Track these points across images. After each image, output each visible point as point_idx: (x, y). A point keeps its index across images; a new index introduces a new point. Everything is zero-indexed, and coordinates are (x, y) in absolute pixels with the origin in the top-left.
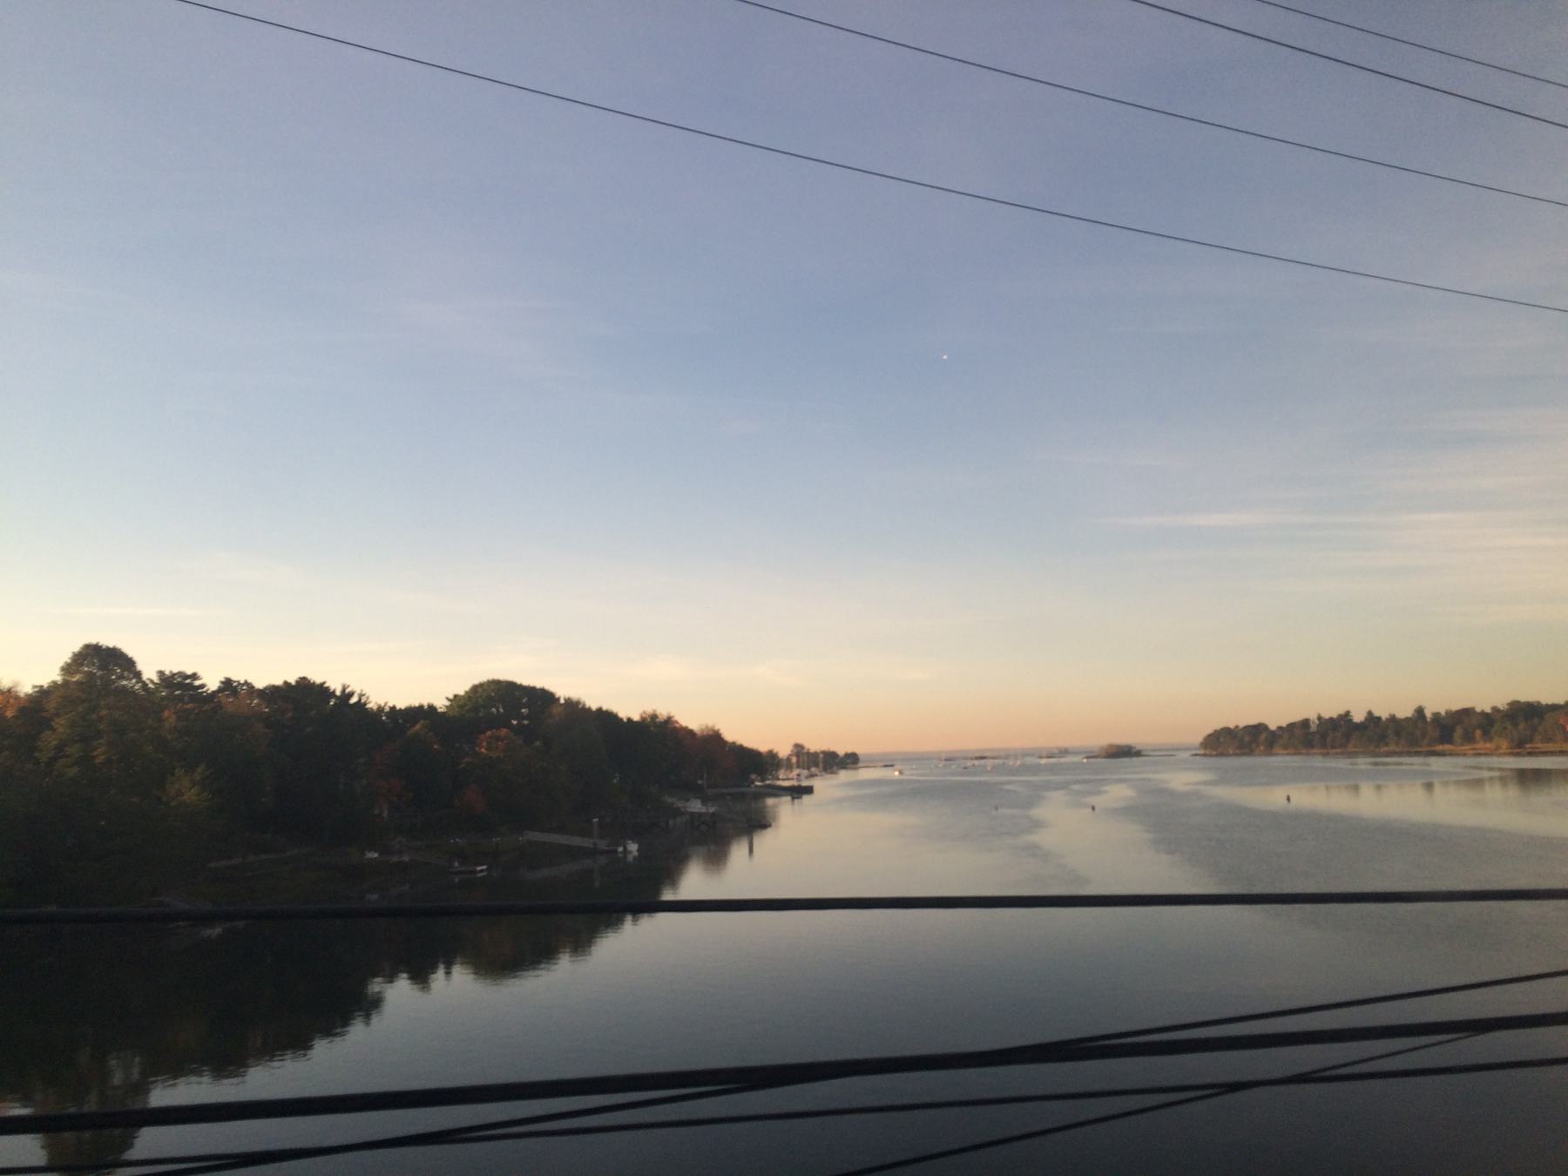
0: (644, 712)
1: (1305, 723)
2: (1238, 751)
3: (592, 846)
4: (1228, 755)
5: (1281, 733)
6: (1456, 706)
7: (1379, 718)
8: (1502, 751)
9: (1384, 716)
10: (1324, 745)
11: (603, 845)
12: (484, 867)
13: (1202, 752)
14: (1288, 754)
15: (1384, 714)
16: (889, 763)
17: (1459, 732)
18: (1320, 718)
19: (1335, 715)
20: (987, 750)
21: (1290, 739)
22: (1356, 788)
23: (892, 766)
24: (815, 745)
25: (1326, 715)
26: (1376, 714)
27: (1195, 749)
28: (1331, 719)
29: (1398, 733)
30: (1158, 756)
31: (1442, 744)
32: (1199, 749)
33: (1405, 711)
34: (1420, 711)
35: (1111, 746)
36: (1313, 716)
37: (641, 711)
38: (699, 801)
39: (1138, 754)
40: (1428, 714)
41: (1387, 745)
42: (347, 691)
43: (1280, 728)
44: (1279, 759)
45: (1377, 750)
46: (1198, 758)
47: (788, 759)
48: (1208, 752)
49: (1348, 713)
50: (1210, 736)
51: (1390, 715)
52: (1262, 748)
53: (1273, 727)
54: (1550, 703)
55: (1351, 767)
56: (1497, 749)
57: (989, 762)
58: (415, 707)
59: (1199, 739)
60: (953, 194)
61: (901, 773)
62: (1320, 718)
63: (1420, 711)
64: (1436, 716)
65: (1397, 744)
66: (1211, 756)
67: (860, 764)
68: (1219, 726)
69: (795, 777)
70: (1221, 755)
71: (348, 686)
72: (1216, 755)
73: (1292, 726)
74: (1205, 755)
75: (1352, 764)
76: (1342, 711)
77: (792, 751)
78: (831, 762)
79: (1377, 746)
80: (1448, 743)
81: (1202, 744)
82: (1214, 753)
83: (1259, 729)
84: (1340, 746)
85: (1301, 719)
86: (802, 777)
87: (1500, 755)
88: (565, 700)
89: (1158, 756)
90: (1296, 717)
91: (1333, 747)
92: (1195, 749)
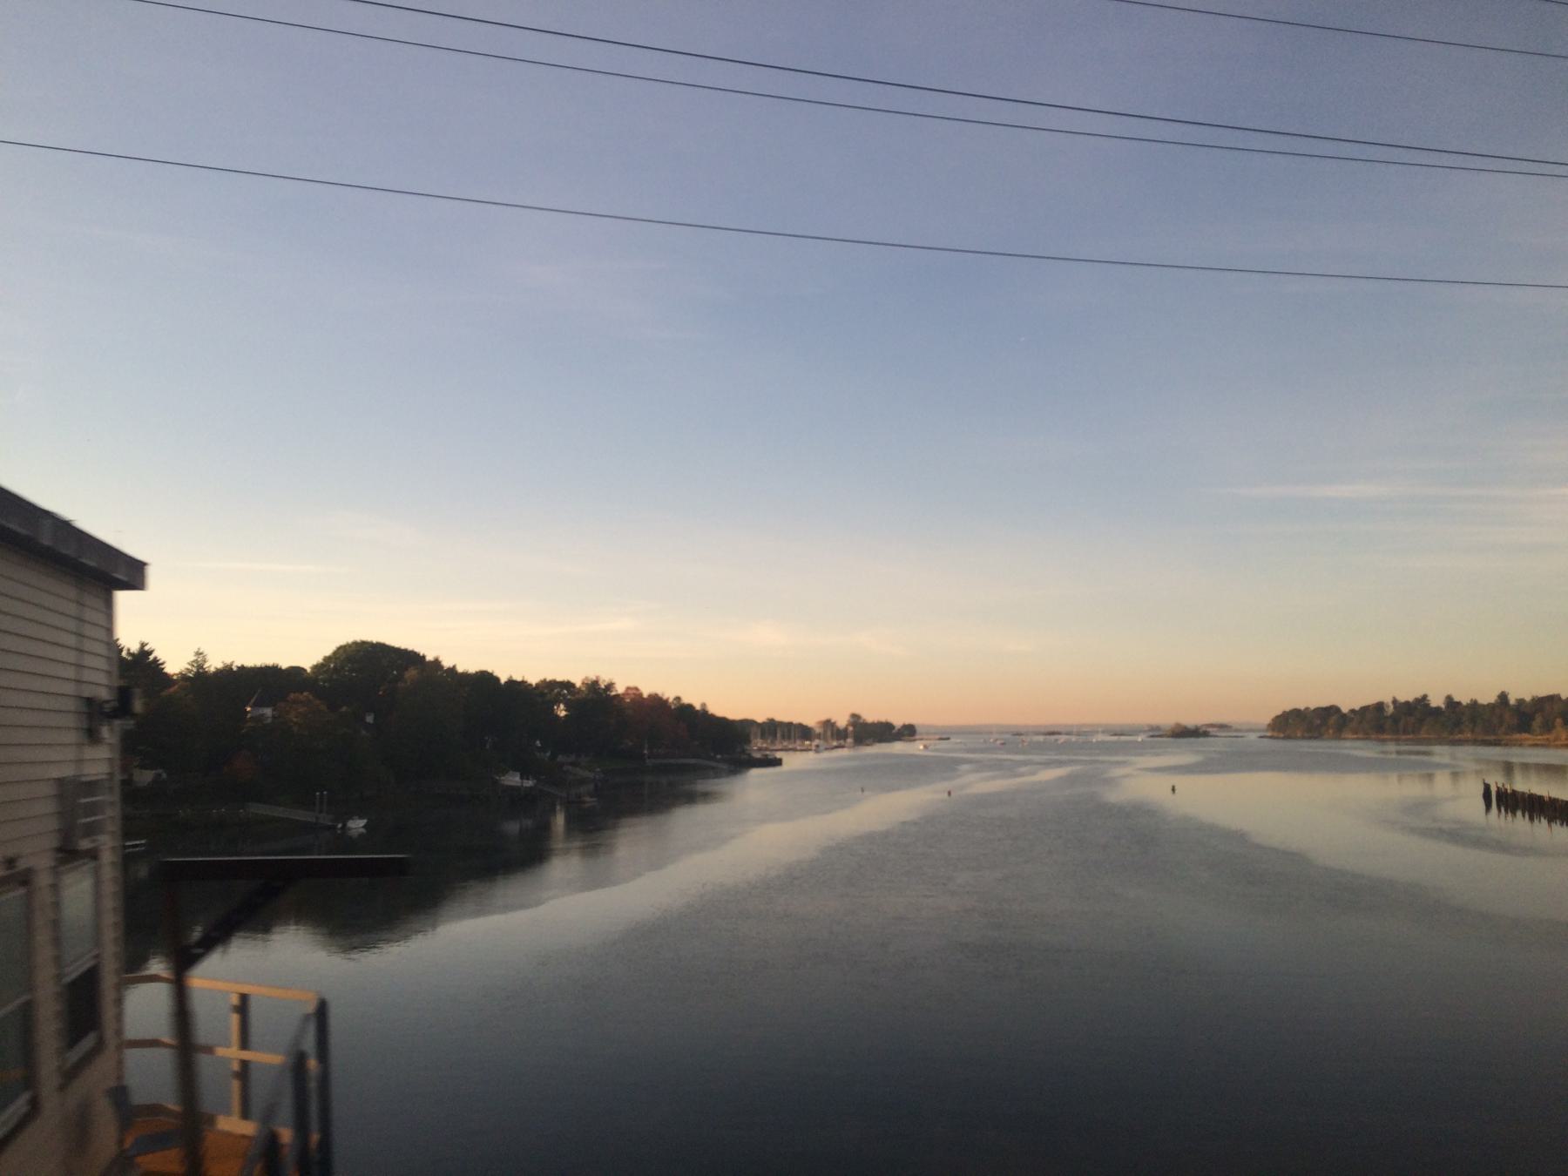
0: (587, 678)
1: (1380, 707)
2: (1306, 735)
3: (314, 820)
4: (1296, 738)
5: (1353, 716)
6: (1543, 692)
7: (1459, 703)
8: (1559, 743)
9: (1465, 700)
10: (1396, 732)
11: (325, 819)
12: (143, 842)
13: (1269, 734)
14: (1358, 739)
15: (1463, 698)
16: (944, 736)
17: (1537, 722)
18: (1395, 701)
19: (1411, 699)
20: (1084, 725)
21: (1361, 722)
22: (1430, 777)
23: (948, 739)
24: (870, 716)
25: (1402, 698)
26: (1456, 699)
27: (1263, 731)
28: (1407, 703)
29: (1473, 720)
30: (1226, 737)
31: (1520, 732)
32: (1267, 730)
33: (1488, 697)
34: (1503, 697)
35: (1178, 725)
36: (1388, 700)
37: (583, 677)
38: (518, 774)
39: (1206, 734)
40: (1512, 701)
41: (1461, 732)
42: (146, 648)
43: (1353, 711)
44: (1348, 744)
45: (1451, 737)
46: (1265, 740)
47: (846, 730)
48: (1275, 734)
49: (1425, 697)
50: (1278, 717)
51: (1472, 700)
52: (1331, 731)
53: (1345, 710)
54: (646, 691)
55: (1382, 756)
56: (1556, 740)
57: (1062, 738)
58: (281, 669)
59: (1266, 718)
60: (600, 75)
61: (925, 747)
62: (1395, 701)
63: (1503, 697)
64: (1521, 702)
65: (1473, 731)
66: (1277, 738)
67: (917, 737)
68: (1288, 708)
69: (814, 748)
70: (1288, 737)
71: (147, 644)
72: (1284, 738)
73: (1365, 709)
74: (1271, 737)
75: (1383, 752)
76: (1419, 695)
77: (849, 721)
78: (1222, 727)
79: (1451, 733)
80: (1525, 732)
81: (1269, 725)
82: (1282, 735)
83: (1330, 712)
84: (1413, 732)
85: (1375, 702)
86: (821, 748)
87: (1557, 747)
88: (155, 658)
89: (1226, 737)
90: (1370, 700)
91: (1405, 732)
92: (1263, 731)
